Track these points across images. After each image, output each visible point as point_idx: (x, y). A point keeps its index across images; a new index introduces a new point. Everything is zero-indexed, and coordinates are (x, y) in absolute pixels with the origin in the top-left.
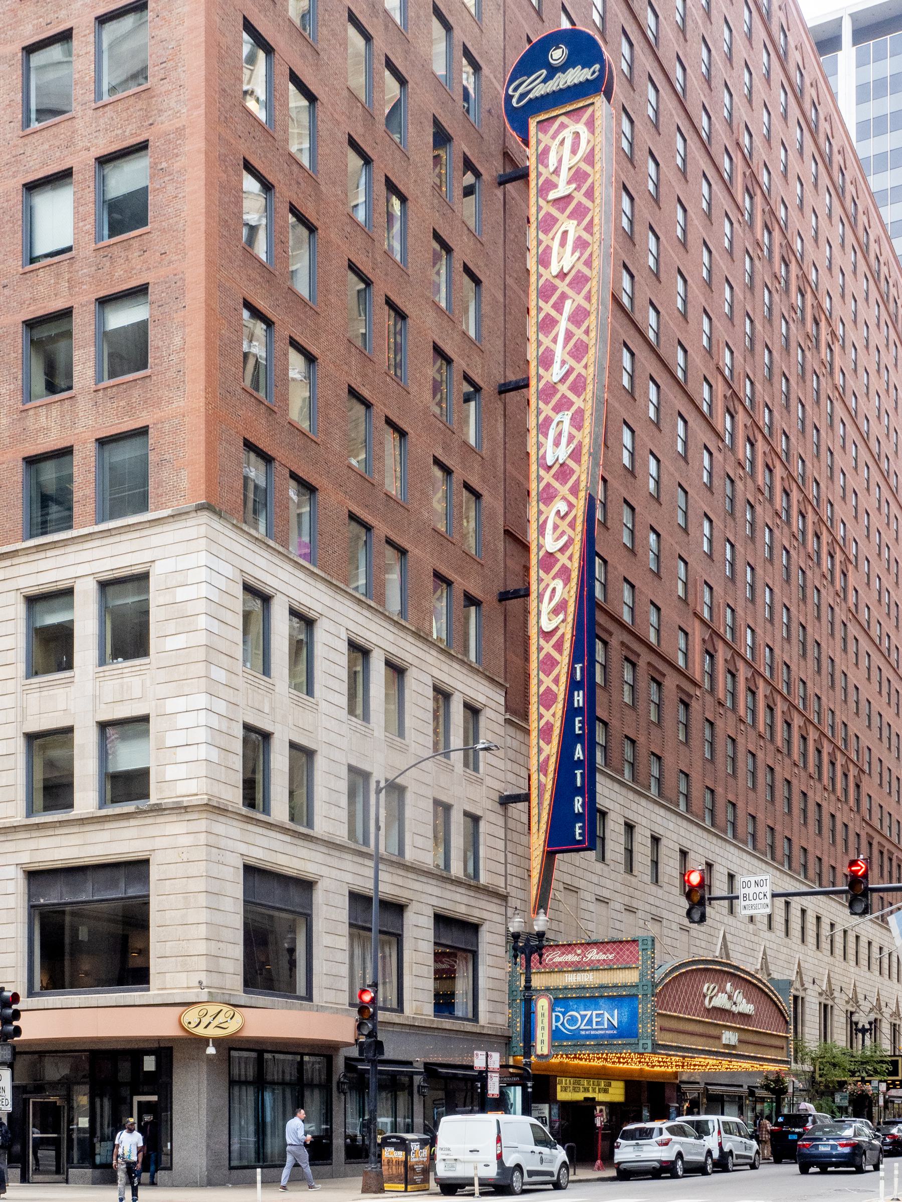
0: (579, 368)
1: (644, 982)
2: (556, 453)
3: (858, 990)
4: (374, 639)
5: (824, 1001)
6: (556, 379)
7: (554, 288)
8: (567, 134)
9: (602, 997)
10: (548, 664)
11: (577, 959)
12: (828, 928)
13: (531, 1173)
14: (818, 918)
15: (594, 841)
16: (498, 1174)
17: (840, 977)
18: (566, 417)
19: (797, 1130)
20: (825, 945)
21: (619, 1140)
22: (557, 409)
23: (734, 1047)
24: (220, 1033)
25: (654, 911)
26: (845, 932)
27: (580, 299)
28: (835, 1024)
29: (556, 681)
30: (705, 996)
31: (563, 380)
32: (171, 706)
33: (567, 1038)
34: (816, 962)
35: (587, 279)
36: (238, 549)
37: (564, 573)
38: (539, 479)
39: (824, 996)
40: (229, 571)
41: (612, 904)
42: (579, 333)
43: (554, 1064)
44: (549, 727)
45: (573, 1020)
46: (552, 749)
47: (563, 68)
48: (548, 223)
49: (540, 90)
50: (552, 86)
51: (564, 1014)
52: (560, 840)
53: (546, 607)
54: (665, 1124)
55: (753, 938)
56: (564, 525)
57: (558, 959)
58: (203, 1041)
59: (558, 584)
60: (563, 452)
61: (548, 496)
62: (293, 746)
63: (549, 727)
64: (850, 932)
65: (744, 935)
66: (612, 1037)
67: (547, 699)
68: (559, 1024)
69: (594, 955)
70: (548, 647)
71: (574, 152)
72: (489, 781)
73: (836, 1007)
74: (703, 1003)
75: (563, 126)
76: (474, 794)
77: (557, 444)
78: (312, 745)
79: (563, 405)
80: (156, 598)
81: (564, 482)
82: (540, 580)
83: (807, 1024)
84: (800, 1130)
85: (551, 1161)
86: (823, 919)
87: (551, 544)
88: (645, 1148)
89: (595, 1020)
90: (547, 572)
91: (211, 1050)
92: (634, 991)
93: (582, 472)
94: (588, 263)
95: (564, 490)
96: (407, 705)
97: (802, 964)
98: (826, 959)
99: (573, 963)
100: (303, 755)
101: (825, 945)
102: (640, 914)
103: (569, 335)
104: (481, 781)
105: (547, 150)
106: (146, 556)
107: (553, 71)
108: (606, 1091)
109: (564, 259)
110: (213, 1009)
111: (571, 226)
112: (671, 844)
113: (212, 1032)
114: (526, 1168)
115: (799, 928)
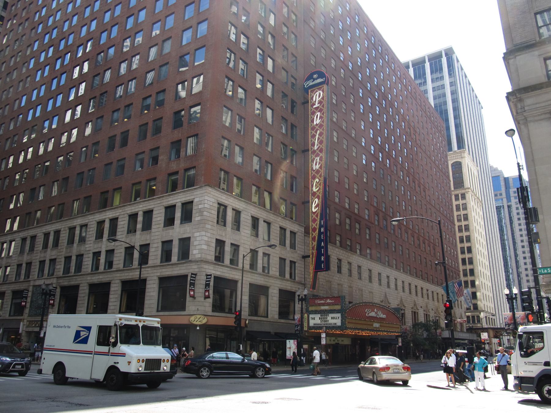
0: (321, 146)
2: (316, 167)
4: (260, 216)
5: (425, 313)
6: (315, 149)
7: (315, 128)
8: (318, 93)
10: (314, 221)
15: (327, 268)
18: (318, 158)
20: (425, 296)
22: (316, 156)
24: (200, 323)
26: (433, 292)
27: (321, 130)
29: (316, 225)
31: (317, 149)
32: (197, 234)
35: (323, 125)
36: (217, 195)
37: (318, 197)
38: (312, 173)
40: (213, 200)
42: (321, 138)
44: (315, 237)
46: (315, 243)
47: (317, 79)
48: (313, 113)
49: (311, 84)
50: (314, 83)
52: (318, 268)
53: (314, 206)
56: (318, 185)
58: (196, 326)
59: (317, 200)
60: (318, 167)
61: (314, 178)
62: (232, 244)
63: (315, 237)
67: (314, 230)
69: (328, 301)
70: (314, 216)
71: (319, 97)
72: (298, 252)
74: (365, 315)
75: (317, 91)
76: (289, 255)
77: (316, 164)
78: (239, 244)
79: (317, 155)
80: (194, 208)
81: (318, 174)
82: (312, 199)
87: (315, 190)
90: (314, 196)
91: (198, 328)
93: (322, 172)
94: (323, 122)
95: (318, 176)
96: (271, 232)
100: (236, 247)
101: (425, 296)
103: (318, 139)
104: (296, 252)
105: (313, 97)
106: (192, 197)
107: (314, 80)
109: (317, 121)
110: (199, 316)
111: (319, 114)
112: (365, 268)
113: (198, 323)
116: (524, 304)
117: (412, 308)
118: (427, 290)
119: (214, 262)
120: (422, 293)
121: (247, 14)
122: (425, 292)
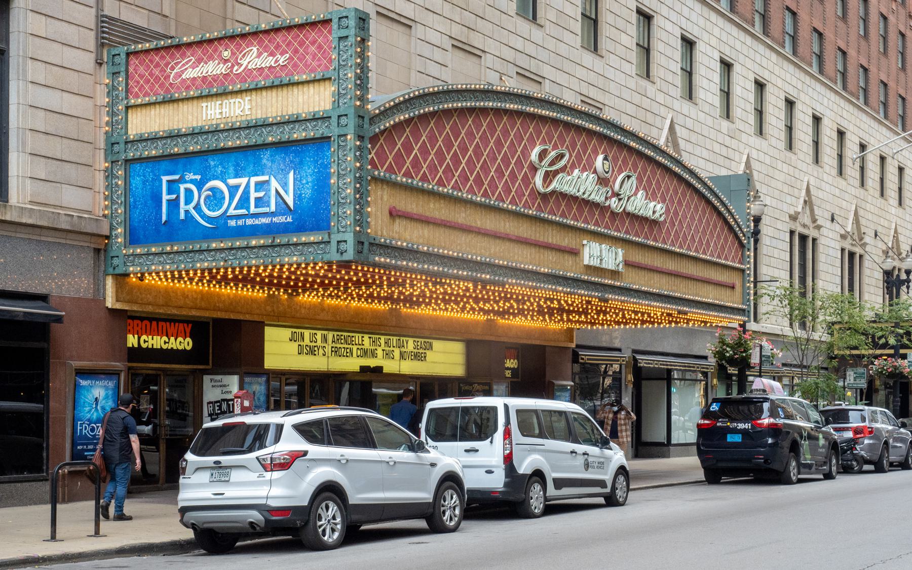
1: (342, 111)
3: (901, 238)
5: (847, 246)
9: (265, 146)
11: (222, 69)
12: (857, 148)
13: (560, 483)
14: (841, 134)
16: (506, 485)
17: (875, 219)
19: (741, 426)
20: (852, 171)
21: (189, 456)
23: (614, 274)
25: (523, 62)
26: (883, 159)
28: (866, 280)
30: (534, 169)
33: (209, 235)
34: (837, 192)
39: (849, 240)
41: (419, 31)
43: (302, 306)
45: (215, 198)
51: (200, 185)
54: (289, 420)
55: (728, 141)
57: (190, 74)
64: (889, 160)
65: (713, 134)
66: (285, 229)
68: (190, 207)
69: (253, 58)
73: (866, 257)
74: (527, 181)
83: (821, 275)
84: (747, 426)
85: (601, 465)
86: (848, 135)
88: (236, 475)
89: (253, 195)
92: (321, 130)
97: (813, 191)
98: (853, 191)
99: (215, 78)
102: (488, 60)
108: (418, 357)
114: (551, 475)
115: (809, 140)
116: (155, 388)
117: (794, 218)
118: (863, 147)
119: (499, 435)
120: (840, 157)
121: (405, 241)
122: (852, 150)
